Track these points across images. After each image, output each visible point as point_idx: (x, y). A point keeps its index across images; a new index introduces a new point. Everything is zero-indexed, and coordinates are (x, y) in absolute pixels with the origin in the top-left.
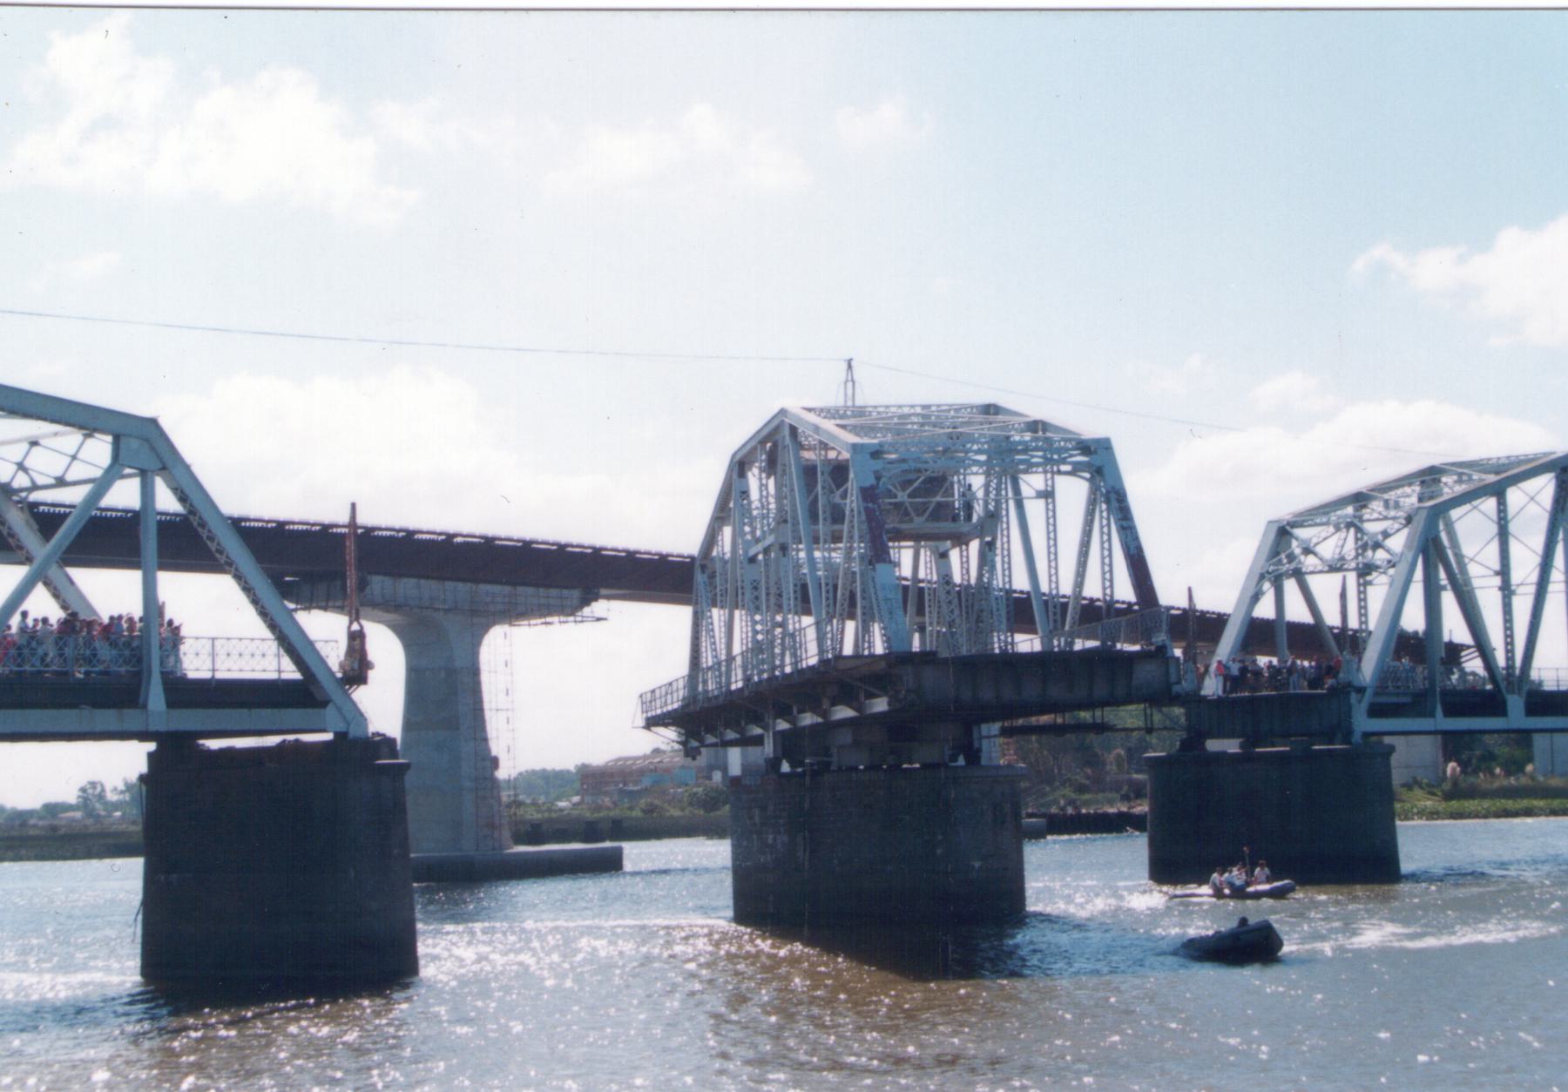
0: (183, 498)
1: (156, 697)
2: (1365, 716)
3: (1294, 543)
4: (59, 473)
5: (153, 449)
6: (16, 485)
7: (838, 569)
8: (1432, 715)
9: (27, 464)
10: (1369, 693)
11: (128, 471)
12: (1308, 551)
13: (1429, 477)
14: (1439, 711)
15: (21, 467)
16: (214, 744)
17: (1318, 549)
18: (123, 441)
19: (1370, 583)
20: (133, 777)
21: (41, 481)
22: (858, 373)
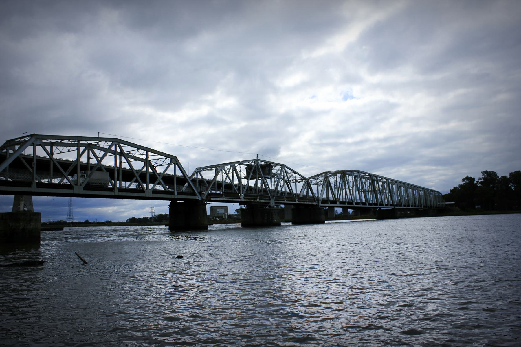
0: (391, 180)
1: (338, 203)
2: (320, 203)
3: (310, 181)
4: (161, 164)
5: (176, 160)
6: (155, 165)
7: (53, 175)
8: (346, 204)
9: (157, 163)
10: (321, 200)
11: (172, 163)
12: (312, 182)
13: (326, 173)
14: (329, 203)
15: (156, 163)
16: (382, 209)
17: (313, 182)
18: (172, 159)
19: (319, 187)
20: (157, 214)
21: (158, 165)
22: (258, 156)
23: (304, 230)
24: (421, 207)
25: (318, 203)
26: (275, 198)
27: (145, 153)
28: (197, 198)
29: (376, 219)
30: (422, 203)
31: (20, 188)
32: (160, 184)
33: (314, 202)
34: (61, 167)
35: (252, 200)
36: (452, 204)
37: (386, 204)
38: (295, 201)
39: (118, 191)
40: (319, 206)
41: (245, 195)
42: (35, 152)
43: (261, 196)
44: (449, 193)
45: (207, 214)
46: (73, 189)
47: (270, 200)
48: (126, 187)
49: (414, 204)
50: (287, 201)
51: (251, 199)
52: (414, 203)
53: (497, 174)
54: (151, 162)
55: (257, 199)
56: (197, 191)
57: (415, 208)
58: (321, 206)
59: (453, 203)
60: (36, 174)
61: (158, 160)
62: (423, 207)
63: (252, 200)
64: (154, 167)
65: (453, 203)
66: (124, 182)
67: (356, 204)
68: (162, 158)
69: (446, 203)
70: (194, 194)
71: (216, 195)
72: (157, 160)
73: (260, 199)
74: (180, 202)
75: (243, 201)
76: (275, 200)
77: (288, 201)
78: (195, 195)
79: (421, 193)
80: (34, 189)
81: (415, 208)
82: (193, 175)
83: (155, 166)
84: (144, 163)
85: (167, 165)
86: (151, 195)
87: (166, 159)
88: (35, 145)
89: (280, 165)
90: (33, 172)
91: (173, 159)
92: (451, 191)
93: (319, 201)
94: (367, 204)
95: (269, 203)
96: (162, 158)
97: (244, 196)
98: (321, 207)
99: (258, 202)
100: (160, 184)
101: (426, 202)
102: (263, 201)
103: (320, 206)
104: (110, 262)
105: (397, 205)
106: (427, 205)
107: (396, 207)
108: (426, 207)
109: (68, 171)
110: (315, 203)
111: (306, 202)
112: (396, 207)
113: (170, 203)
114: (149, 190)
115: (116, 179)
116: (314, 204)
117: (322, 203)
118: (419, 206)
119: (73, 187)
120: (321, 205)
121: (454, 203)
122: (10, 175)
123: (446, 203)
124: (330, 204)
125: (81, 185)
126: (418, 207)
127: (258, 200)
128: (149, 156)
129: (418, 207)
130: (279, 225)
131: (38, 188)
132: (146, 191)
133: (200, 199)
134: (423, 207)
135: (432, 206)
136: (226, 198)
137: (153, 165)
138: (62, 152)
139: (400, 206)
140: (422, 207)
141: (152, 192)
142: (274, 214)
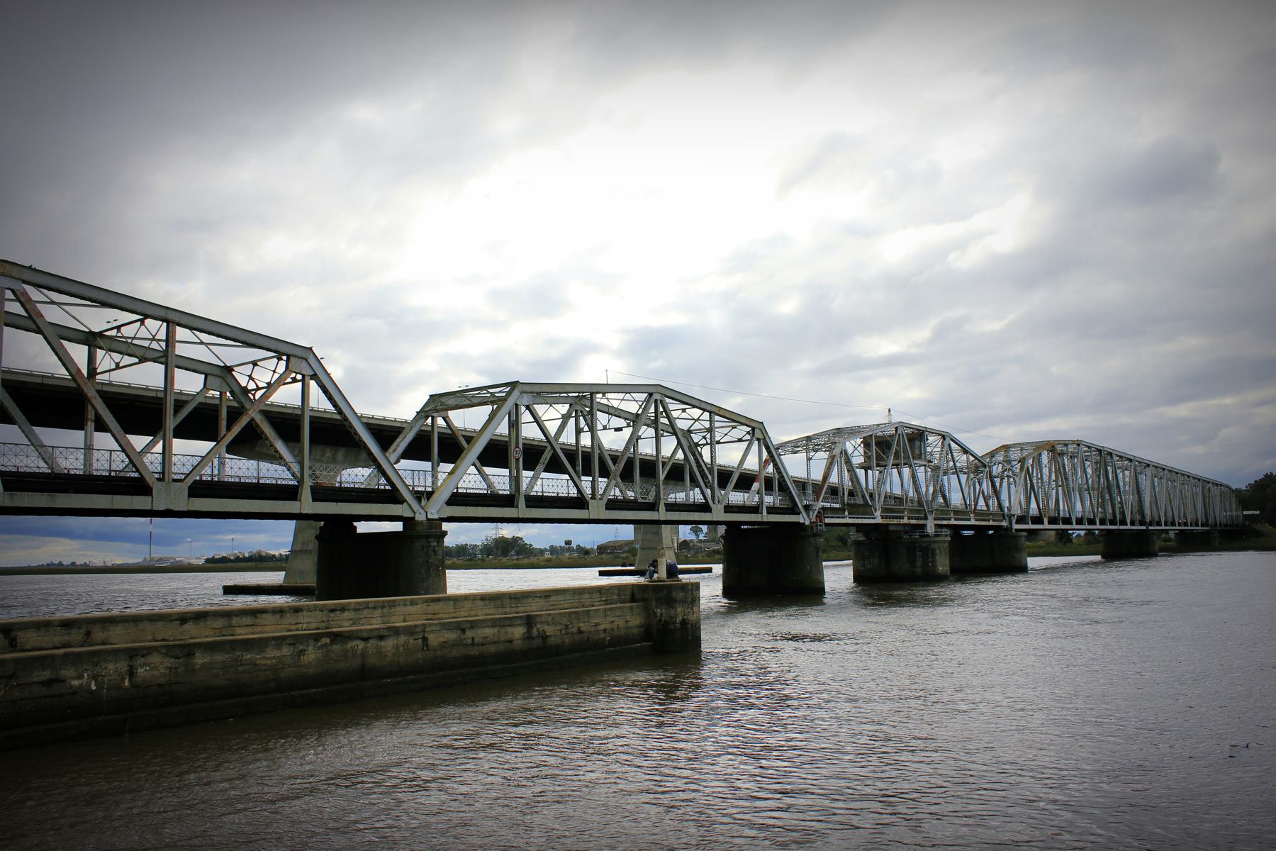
6: (249, 388)
9: (253, 376)
15: (251, 377)
23: (1072, 577)
24: (1197, 525)
25: (1010, 522)
26: (935, 514)
27: (706, 415)
28: (802, 521)
29: (1098, 558)
30: (1199, 517)
31: (462, 508)
33: (1002, 521)
34: (18, 405)
35: (895, 521)
36: (1253, 515)
37: (1077, 519)
38: (969, 520)
40: (1012, 529)
41: (884, 510)
42: (306, 398)
43: (911, 511)
44: (1244, 488)
45: (450, 574)
47: (926, 518)
48: (110, 471)
49: (1138, 517)
50: (976, 520)
51: (893, 517)
54: (233, 373)
55: (902, 518)
56: (801, 504)
57: (1122, 527)
58: (1017, 530)
59: (1255, 512)
61: (255, 364)
62: (1128, 521)
63: (895, 521)
64: (250, 395)
65: (1255, 512)
66: (252, 462)
67: (1050, 523)
68: (722, 427)
69: (1245, 513)
71: (831, 509)
72: (251, 366)
73: (909, 518)
74: (748, 529)
75: (880, 524)
76: (935, 519)
77: (963, 520)
79: (1124, 475)
80: (662, 514)
81: (1122, 527)
83: (699, 445)
84: (204, 376)
85: (748, 442)
86: (182, 502)
87: (734, 427)
88: (307, 378)
89: (940, 435)
90: (713, 481)
91: (293, 356)
93: (1012, 518)
94: (1046, 520)
95: (924, 526)
96: (722, 427)
97: (882, 512)
99: (905, 524)
101: (1206, 516)
102: (914, 522)
103: (1014, 531)
104: (275, 753)
105: (1151, 524)
106: (1207, 520)
107: (1150, 528)
108: (1207, 526)
109: (543, 463)
110: (1004, 524)
111: (989, 520)
112: (1150, 528)
115: (597, 474)
116: (1003, 526)
117: (1017, 523)
118: (1137, 522)
119: (588, 503)
120: (1016, 526)
121: (1258, 512)
122: (314, 471)
123: (1245, 513)
124: (1063, 524)
125: (600, 499)
126: (1133, 523)
127: (905, 521)
128: (177, 344)
129: (1166, 525)
130: (1023, 569)
132: (156, 487)
133: (807, 523)
134: (1128, 521)
135: (1218, 523)
136: (850, 518)
137: (243, 385)
138: (121, 365)
139: (1110, 524)
141: (604, 506)
142: (938, 552)
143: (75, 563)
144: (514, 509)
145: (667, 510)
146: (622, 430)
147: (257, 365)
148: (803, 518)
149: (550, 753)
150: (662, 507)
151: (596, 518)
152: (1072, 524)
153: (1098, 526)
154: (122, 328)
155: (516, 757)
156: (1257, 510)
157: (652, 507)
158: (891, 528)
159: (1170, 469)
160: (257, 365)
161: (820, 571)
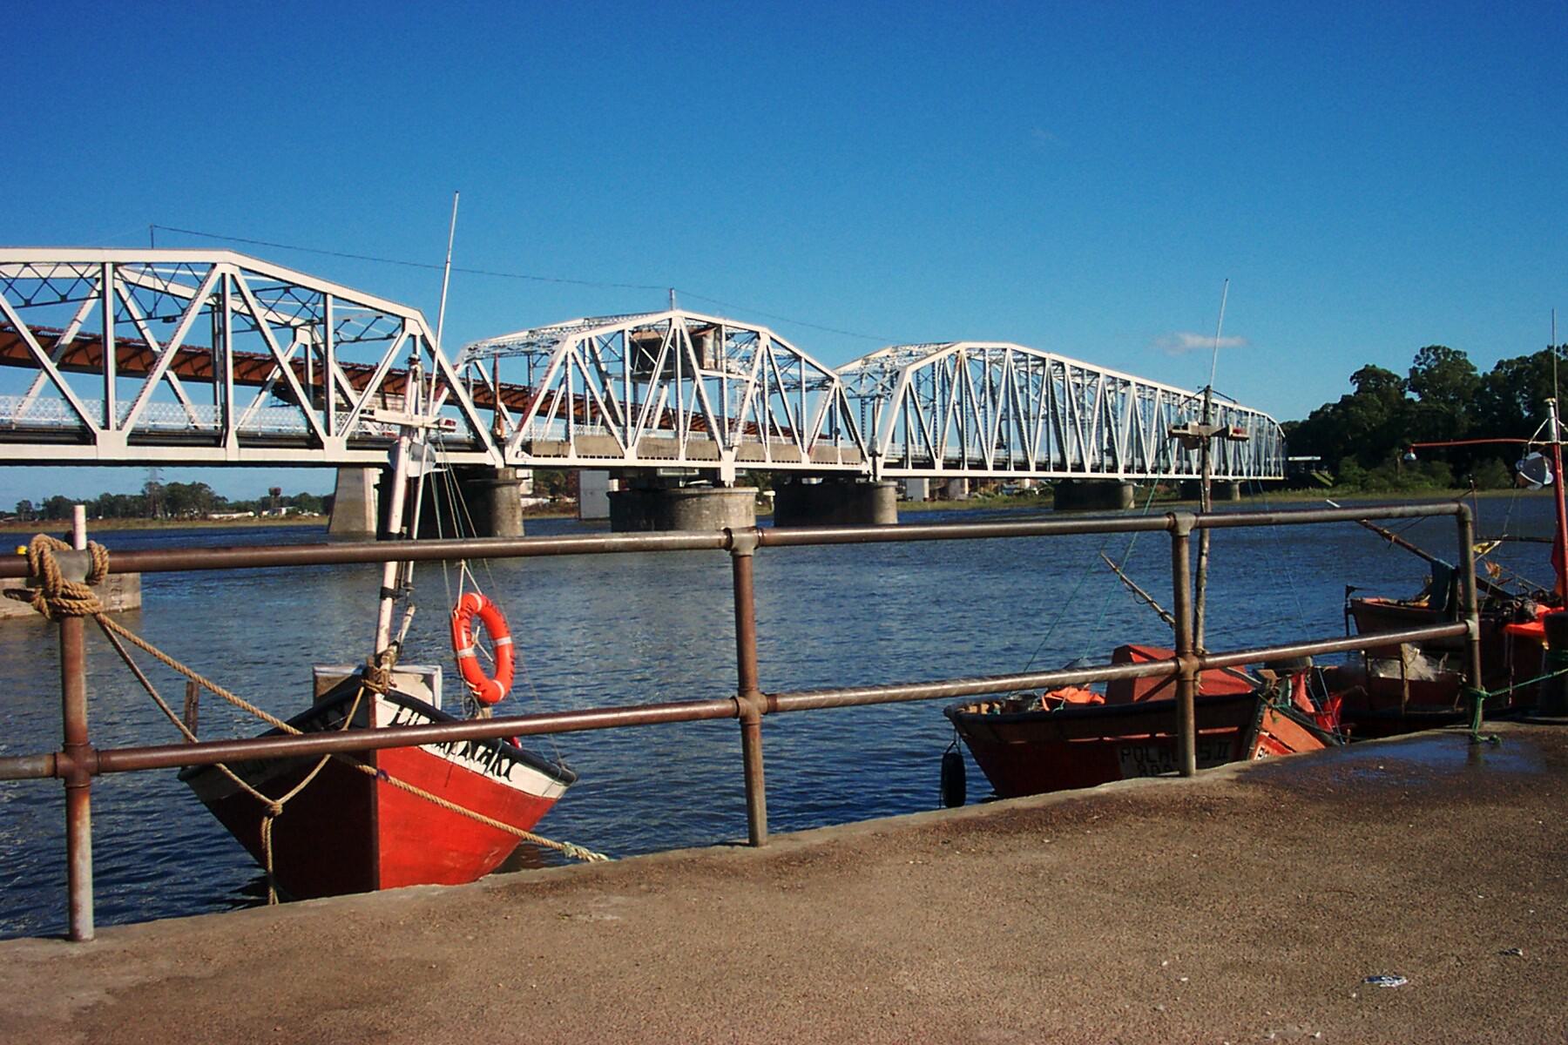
28: (489, 462)
32: (169, 501)
39: (237, 446)
46: (95, 443)
52: (1078, 458)
53: (1374, 366)
60: (694, 528)
67: (1038, 469)
70: (477, 446)
78: (1538, 438)
82: (308, 431)
92: (1313, 415)
93: (878, 459)
98: (886, 483)
100: (169, 501)
113: (381, 475)
114: (13, 546)
125: (118, 428)
126: (1127, 470)
129: (1154, 471)
131: (131, 447)
133: (500, 465)
140: (1192, 473)
143: (28, 503)
144: (221, 450)
145: (241, 446)
146: (174, 320)
147: (26, 301)
148: (491, 457)
149: (119, 839)
150: (232, 440)
151: (223, 459)
152: (985, 468)
153: (1033, 473)
154: (258, 332)
155: (704, 617)
156: (1317, 456)
157: (217, 439)
158: (661, 473)
159: (527, 875)
160: (26, 301)
161: (142, 601)
